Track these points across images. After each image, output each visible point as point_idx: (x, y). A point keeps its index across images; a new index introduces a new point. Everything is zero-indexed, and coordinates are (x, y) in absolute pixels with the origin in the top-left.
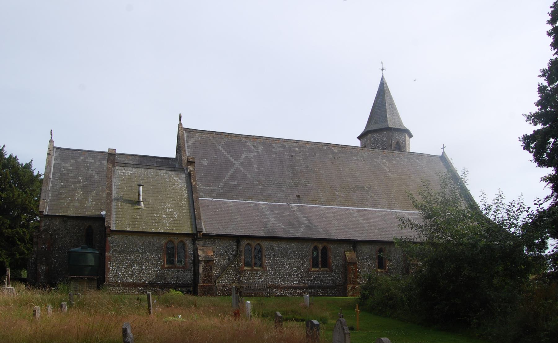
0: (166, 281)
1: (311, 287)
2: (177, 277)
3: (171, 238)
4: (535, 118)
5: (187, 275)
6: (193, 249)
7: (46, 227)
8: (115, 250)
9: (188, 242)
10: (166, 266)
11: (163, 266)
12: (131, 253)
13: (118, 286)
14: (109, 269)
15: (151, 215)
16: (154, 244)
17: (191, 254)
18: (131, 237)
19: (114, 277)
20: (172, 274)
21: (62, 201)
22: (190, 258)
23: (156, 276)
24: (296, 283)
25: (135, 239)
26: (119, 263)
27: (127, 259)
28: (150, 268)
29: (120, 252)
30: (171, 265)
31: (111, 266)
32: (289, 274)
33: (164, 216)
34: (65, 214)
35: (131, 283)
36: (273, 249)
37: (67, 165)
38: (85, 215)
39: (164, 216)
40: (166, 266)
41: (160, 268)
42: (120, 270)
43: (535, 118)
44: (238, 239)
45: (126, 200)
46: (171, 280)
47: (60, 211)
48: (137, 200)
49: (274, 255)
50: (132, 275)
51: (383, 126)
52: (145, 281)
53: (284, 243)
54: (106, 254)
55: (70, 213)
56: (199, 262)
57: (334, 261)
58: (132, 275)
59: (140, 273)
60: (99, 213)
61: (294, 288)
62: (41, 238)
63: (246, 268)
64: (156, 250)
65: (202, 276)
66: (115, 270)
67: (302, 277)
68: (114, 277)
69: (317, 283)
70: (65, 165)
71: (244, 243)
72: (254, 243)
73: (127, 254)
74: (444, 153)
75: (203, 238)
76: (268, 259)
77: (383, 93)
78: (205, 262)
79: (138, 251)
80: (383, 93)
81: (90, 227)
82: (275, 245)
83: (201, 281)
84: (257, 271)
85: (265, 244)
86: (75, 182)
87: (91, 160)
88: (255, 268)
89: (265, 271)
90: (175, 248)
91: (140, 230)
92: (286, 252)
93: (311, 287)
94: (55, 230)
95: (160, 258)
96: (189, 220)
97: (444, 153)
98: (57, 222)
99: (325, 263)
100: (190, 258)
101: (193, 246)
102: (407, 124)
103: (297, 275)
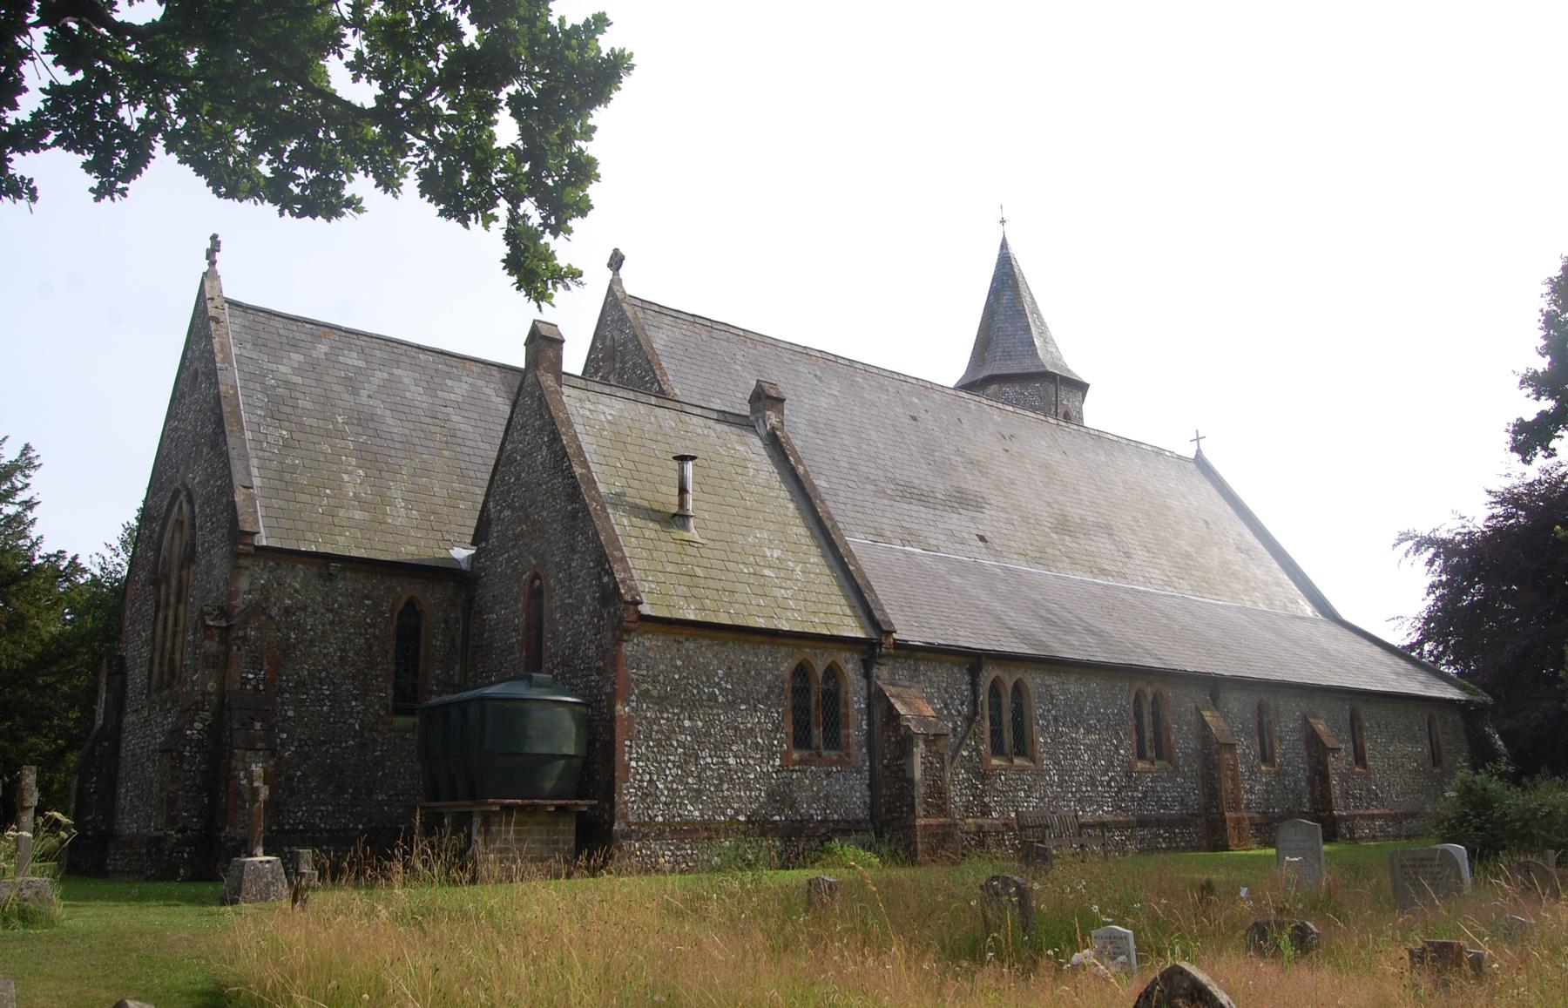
0: (797, 811)
1: (1142, 823)
2: (826, 797)
3: (807, 652)
4: (1538, 384)
5: (852, 788)
6: (864, 693)
7: (257, 596)
8: (645, 695)
9: (850, 668)
10: (796, 756)
11: (785, 756)
12: (692, 706)
13: (660, 836)
14: (628, 766)
15: (731, 566)
16: (758, 674)
17: (859, 710)
18: (691, 645)
19: (643, 800)
20: (811, 785)
21: (304, 498)
22: (859, 728)
23: (768, 795)
24: (1105, 812)
25: (706, 653)
26: (658, 743)
27: (683, 729)
28: (748, 762)
29: (662, 702)
30: (806, 753)
31: (634, 759)
32: (1092, 782)
33: (766, 572)
34: (328, 549)
35: (694, 822)
36: (1052, 697)
37: (282, 368)
38: (401, 558)
39: (766, 572)
40: (796, 756)
41: (778, 762)
42: (661, 772)
43: (1538, 384)
44: (974, 660)
45: (637, 507)
46: (809, 806)
47: (309, 535)
48: (675, 510)
49: (1056, 719)
50: (699, 792)
51: (1027, 366)
52: (737, 813)
53: (1074, 678)
54: (619, 707)
55: (345, 544)
56: (905, 743)
57: (1182, 741)
58: (699, 792)
59: (722, 782)
60: (443, 554)
61: (1103, 825)
62: (245, 639)
63: (995, 762)
64: (767, 696)
65: (922, 790)
66: (648, 777)
67: (1120, 791)
68: (643, 800)
69: (1150, 810)
70: (274, 367)
71: (989, 674)
72: (1009, 678)
73: (682, 709)
74: (1199, 451)
75: (894, 657)
76: (1044, 729)
77: (1007, 280)
78: (926, 742)
79: (713, 697)
80: (1007, 280)
81: (411, 604)
82: (1054, 683)
83: (920, 810)
84: (1022, 770)
85: (1034, 681)
86: (327, 434)
87: (352, 359)
88: (1017, 761)
89: (1040, 773)
90: (828, 688)
91: (724, 619)
92: (1081, 710)
93: (1142, 823)
94: (288, 611)
95: (777, 729)
96: (836, 590)
97: (1199, 451)
98: (296, 580)
99: (1161, 749)
100: (859, 728)
101: (863, 683)
102: (1077, 366)
103: (1109, 783)
